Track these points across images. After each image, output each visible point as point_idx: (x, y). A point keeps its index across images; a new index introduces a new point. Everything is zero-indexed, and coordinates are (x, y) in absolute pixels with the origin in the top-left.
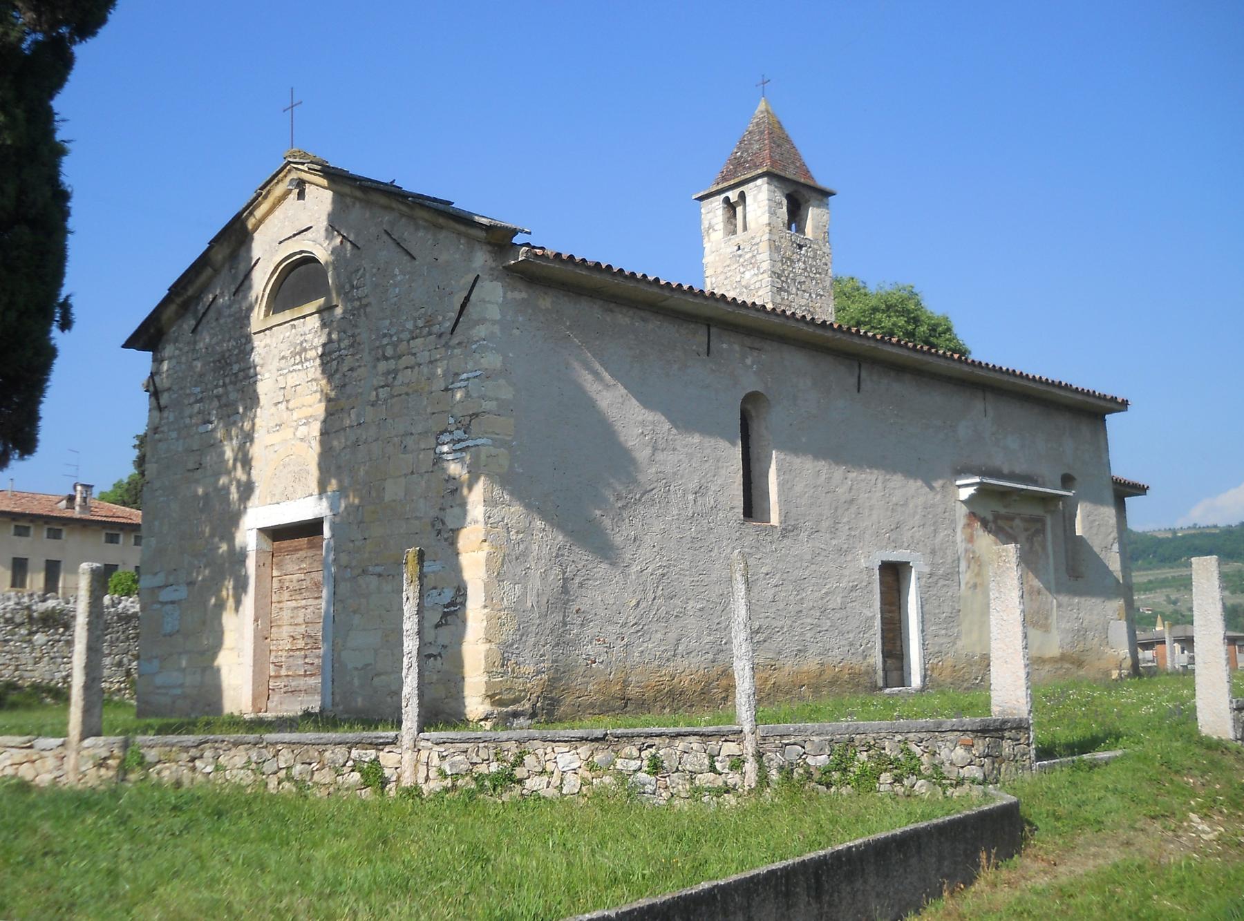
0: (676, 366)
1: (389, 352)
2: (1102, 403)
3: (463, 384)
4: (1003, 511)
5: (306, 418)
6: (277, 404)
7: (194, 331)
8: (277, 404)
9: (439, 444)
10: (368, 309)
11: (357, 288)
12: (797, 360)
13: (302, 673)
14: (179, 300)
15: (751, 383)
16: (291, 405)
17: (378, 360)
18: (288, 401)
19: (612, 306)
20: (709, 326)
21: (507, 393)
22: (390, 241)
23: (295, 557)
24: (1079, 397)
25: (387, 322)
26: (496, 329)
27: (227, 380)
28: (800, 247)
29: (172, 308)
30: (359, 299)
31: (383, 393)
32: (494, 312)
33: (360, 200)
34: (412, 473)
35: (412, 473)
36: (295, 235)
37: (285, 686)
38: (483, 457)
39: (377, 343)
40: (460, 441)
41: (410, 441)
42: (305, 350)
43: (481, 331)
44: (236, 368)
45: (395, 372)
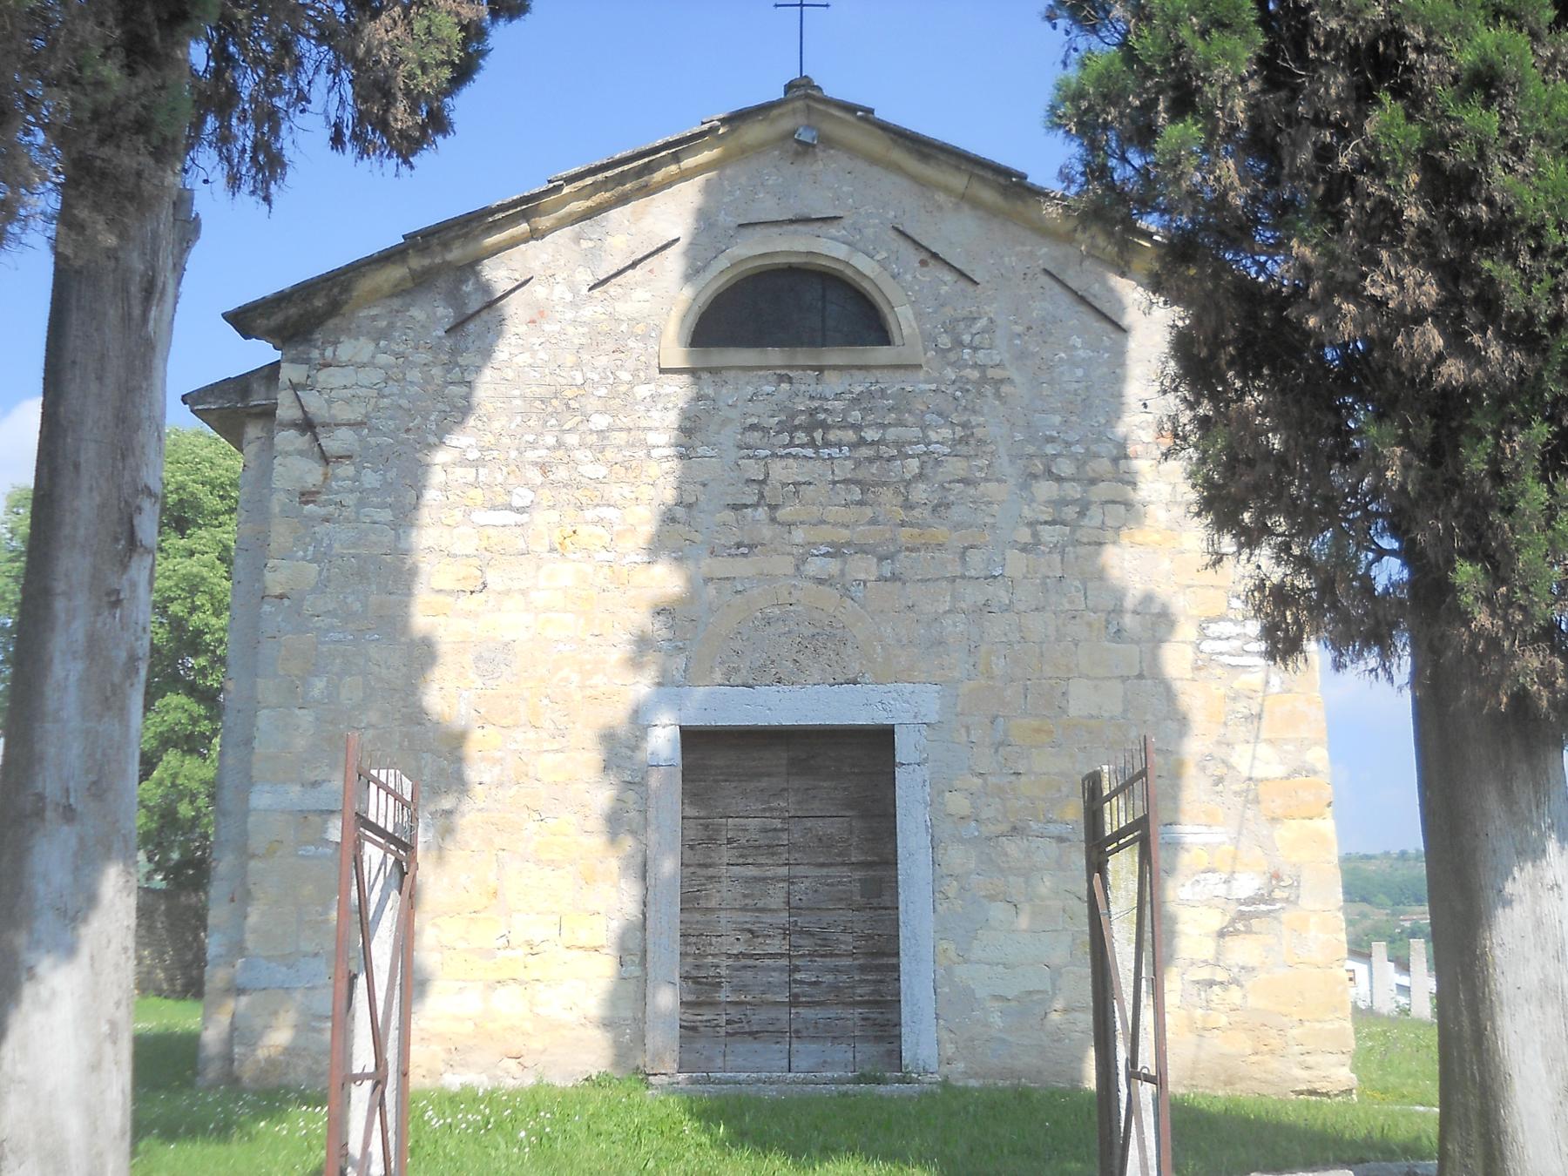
1: (1065, 467)
10: (1005, 389)
17: (1035, 477)
23: (752, 785)
25: (1057, 419)
29: (396, 273)
31: (1049, 534)
34: (1140, 676)
35: (1140, 676)
36: (791, 222)
37: (728, 1022)
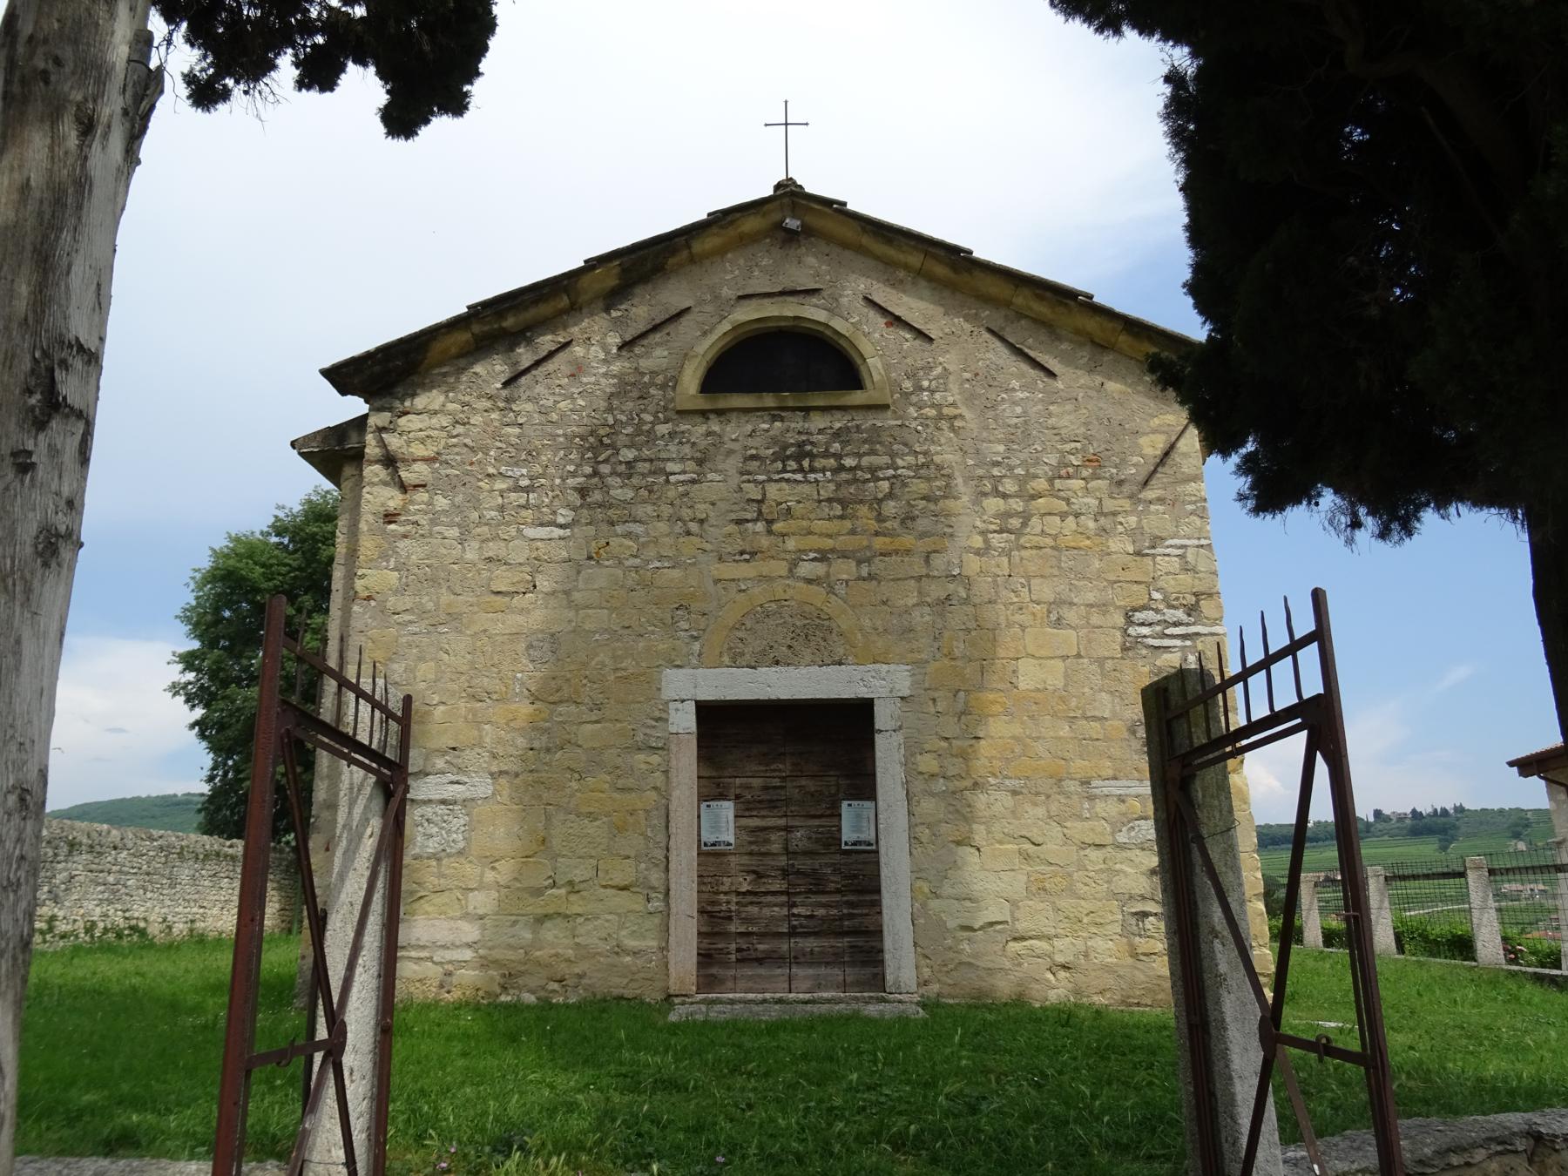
1: (1009, 486)
10: (957, 423)
14: (477, 328)
17: (985, 494)
18: (770, 522)
29: (463, 337)
34: (1079, 656)
35: (1079, 656)
36: (783, 293)
40: (1176, 624)
41: (1071, 615)
45: (1026, 518)
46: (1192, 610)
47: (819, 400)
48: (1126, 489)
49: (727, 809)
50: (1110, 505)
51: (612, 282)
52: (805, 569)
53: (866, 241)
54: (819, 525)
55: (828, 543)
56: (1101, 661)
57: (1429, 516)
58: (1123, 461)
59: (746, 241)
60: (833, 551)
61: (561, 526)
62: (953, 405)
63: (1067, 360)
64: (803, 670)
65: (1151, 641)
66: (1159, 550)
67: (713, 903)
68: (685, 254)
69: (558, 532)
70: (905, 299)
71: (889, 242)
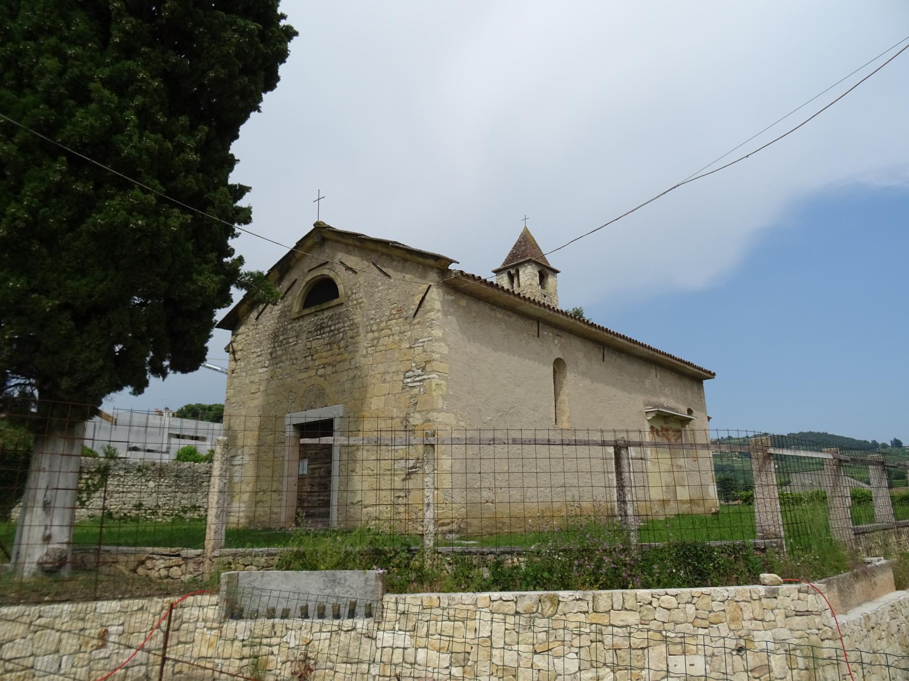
0: (524, 342)
1: (375, 328)
2: (705, 374)
3: (421, 344)
4: (665, 426)
5: (323, 364)
6: (305, 357)
7: (257, 319)
8: (305, 357)
9: (405, 378)
10: (362, 305)
11: (356, 294)
12: (576, 343)
13: (317, 505)
14: (248, 302)
15: (558, 354)
16: (314, 357)
17: (368, 332)
18: (312, 356)
19: (495, 307)
20: (538, 322)
21: (445, 350)
22: (375, 268)
24: (696, 370)
25: (374, 312)
26: (440, 314)
27: (276, 345)
28: (545, 296)
29: (245, 306)
30: (356, 300)
32: (438, 305)
33: (358, 247)
34: (389, 394)
35: (389, 394)
36: (318, 266)
38: (434, 385)
39: (367, 323)
40: (419, 376)
41: (388, 377)
42: (323, 328)
43: (432, 315)
44: (281, 338)
45: (378, 339)
46: (423, 369)
47: (325, 306)
48: (408, 320)
49: (306, 462)
50: (403, 329)
51: (278, 276)
52: (321, 372)
53: (339, 238)
54: (325, 354)
55: (325, 361)
56: (395, 395)
57: (103, 400)
58: (409, 308)
59: (309, 250)
60: (326, 364)
61: (266, 367)
62: (361, 298)
63: (395, 270)
64: (318, 410)
65: (410, 385)
66: (417, 345)
67: (301, 496)
68: (294, 259)
69: (265, 369)
70: (351, 257)
71: (343, 237)
